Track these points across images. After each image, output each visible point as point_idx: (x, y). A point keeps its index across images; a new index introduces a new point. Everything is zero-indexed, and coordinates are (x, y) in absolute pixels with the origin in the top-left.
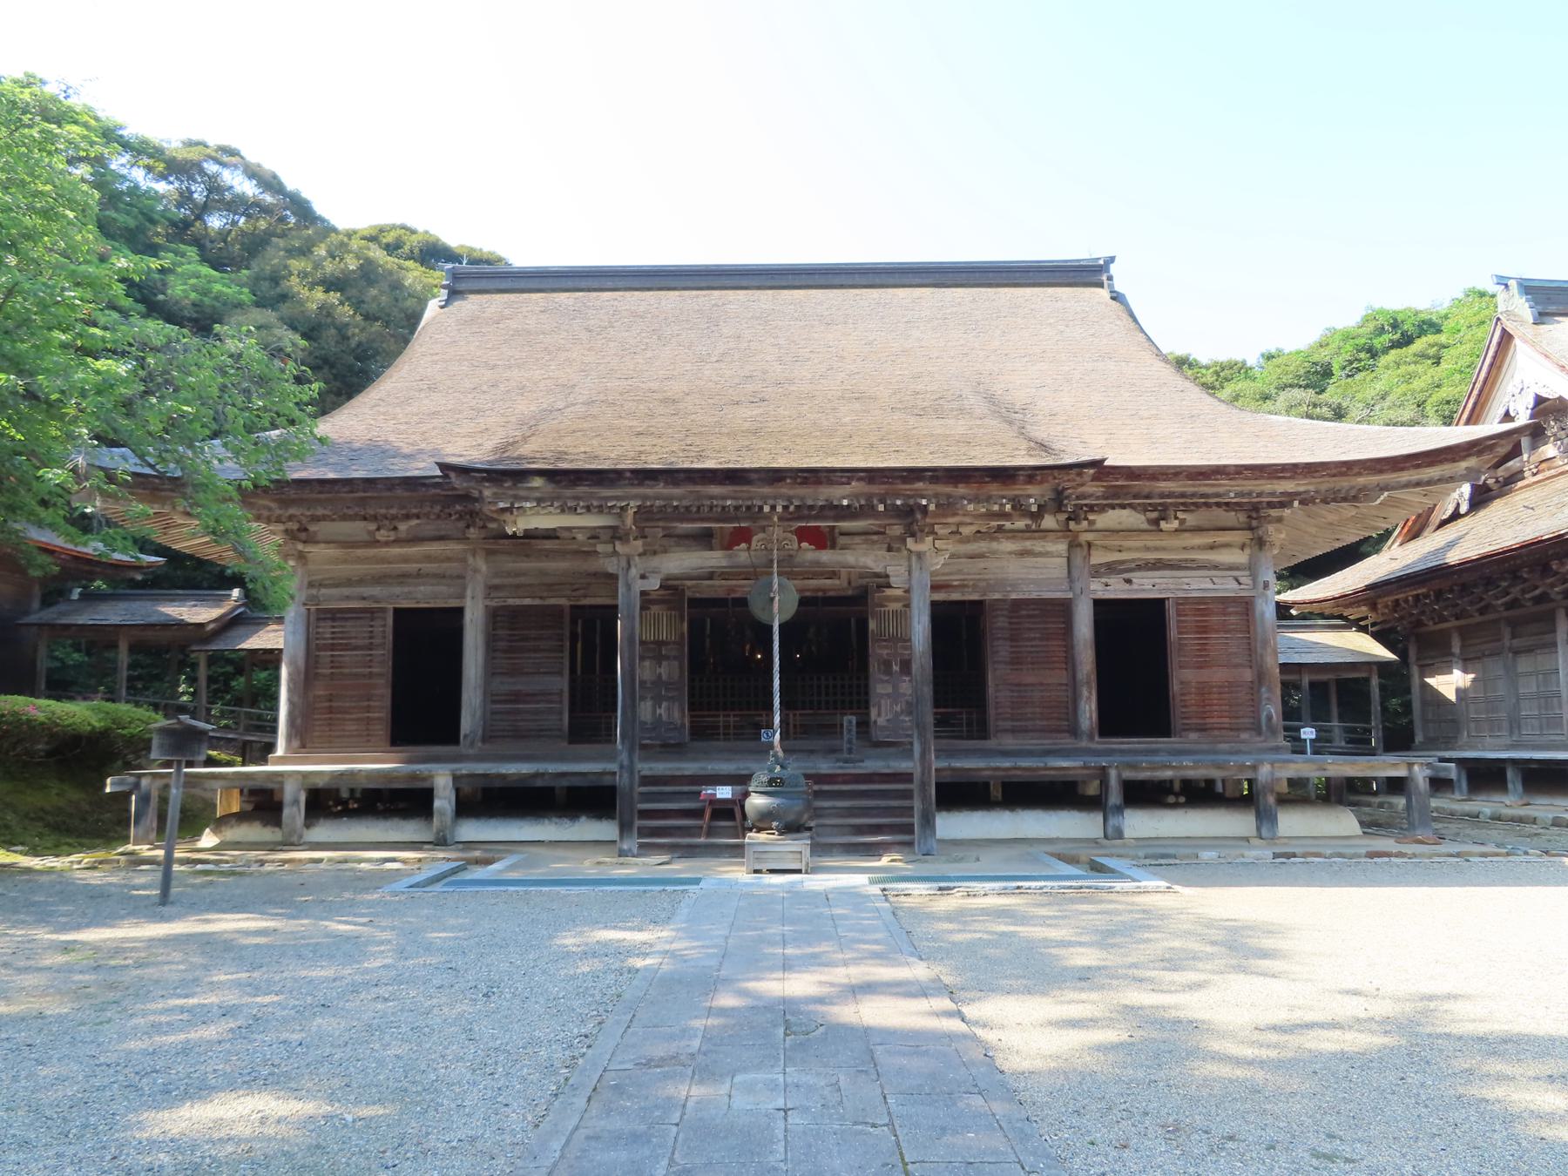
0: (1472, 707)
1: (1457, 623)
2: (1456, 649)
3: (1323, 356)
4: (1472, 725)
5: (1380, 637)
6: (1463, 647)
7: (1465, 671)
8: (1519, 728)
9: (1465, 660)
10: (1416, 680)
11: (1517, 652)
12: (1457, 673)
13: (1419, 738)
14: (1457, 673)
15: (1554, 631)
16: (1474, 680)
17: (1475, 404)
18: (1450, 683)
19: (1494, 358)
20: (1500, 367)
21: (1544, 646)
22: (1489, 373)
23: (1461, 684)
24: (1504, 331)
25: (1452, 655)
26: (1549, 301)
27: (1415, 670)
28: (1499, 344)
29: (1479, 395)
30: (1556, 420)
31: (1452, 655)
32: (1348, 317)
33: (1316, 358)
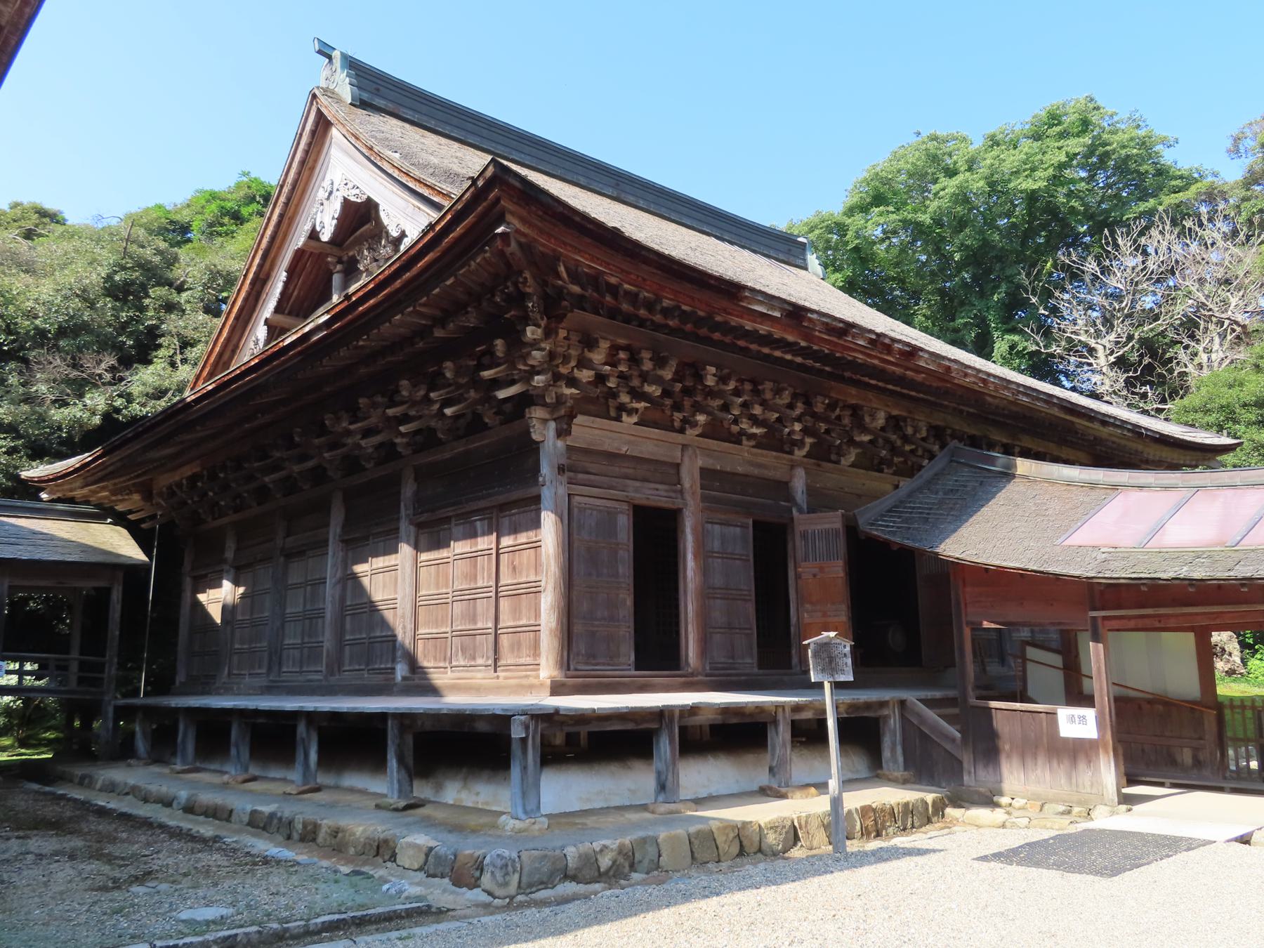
0: (238, 633)
1: (233, 517)
2: (229, 555)
3: (184, 217)
4: (235, 658)
5: (143, 540)
6: (238, 550)
7: (236, 583)
8: (280, 664)
9: (420, 526)
10: (187, 594)
11: (290, 555)
12: (227, 585)
13: (180, 678)
14: (227, 585)
15: (328, 525)
16: (243, 596)
17: (281, 216)
18: (219, 598)
19: (307, 152)
20: (312, 169)
21: (388, 533)
22: (299, 173)
23: (229, 600)
24: (320, 114)
25: (224, 561)
26: (377, 92)
27: (188, 582)
28: (313, 133)
29: (286, 204)
30: (369, 249)
31: (224, 561)
32: (224, 180)
33: (178, 217)
